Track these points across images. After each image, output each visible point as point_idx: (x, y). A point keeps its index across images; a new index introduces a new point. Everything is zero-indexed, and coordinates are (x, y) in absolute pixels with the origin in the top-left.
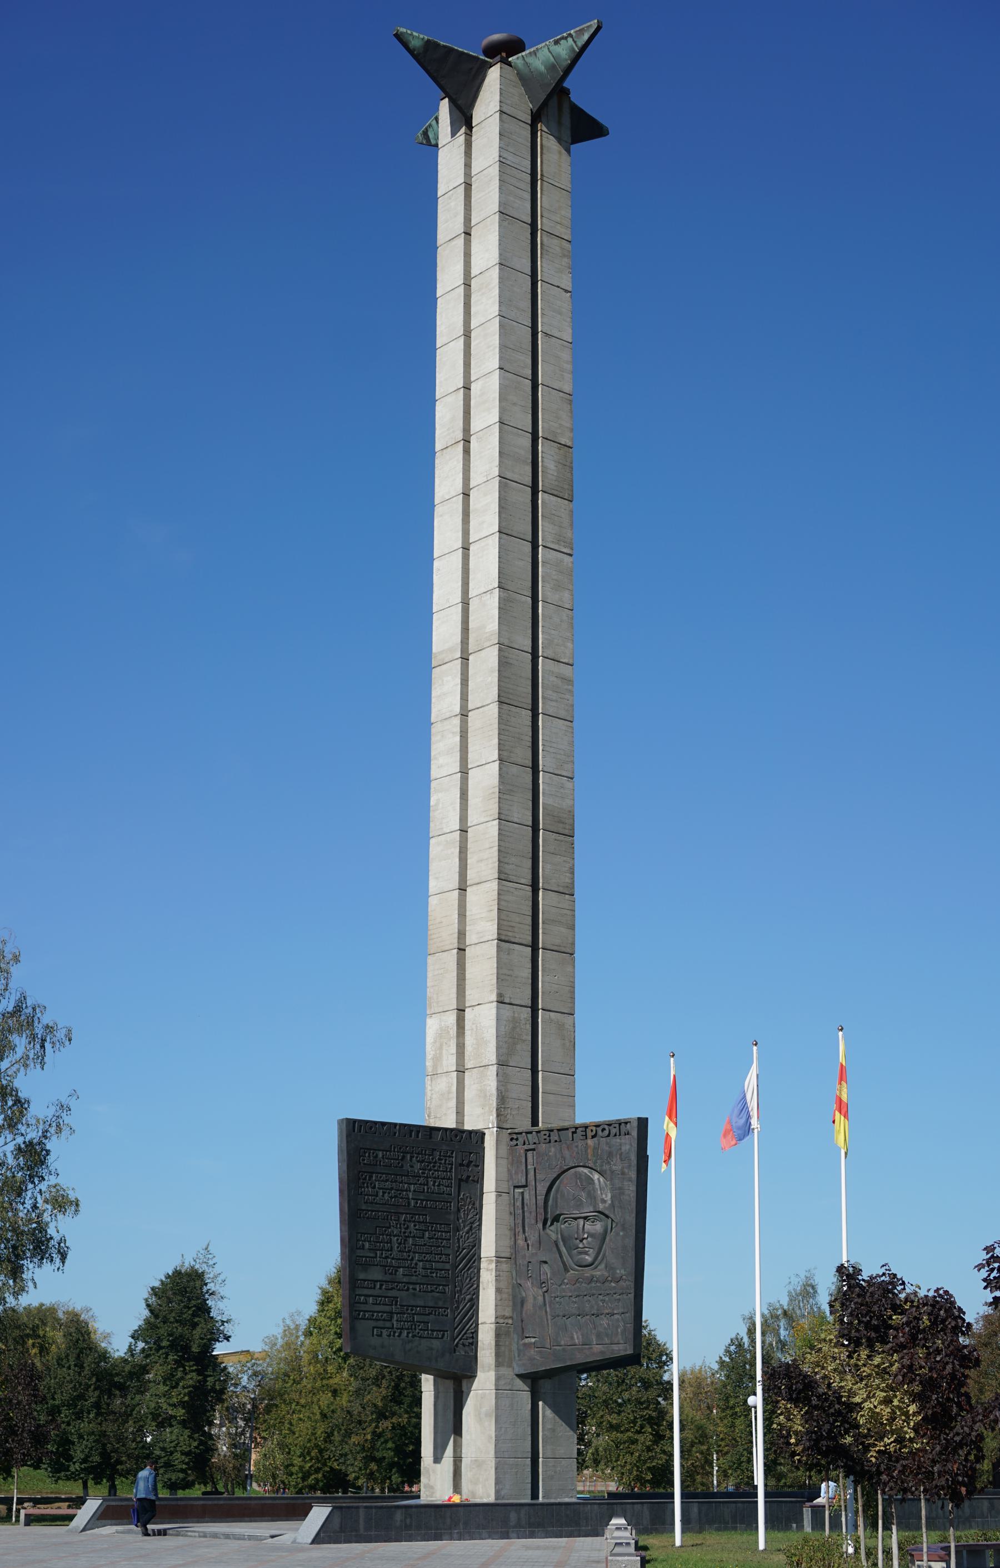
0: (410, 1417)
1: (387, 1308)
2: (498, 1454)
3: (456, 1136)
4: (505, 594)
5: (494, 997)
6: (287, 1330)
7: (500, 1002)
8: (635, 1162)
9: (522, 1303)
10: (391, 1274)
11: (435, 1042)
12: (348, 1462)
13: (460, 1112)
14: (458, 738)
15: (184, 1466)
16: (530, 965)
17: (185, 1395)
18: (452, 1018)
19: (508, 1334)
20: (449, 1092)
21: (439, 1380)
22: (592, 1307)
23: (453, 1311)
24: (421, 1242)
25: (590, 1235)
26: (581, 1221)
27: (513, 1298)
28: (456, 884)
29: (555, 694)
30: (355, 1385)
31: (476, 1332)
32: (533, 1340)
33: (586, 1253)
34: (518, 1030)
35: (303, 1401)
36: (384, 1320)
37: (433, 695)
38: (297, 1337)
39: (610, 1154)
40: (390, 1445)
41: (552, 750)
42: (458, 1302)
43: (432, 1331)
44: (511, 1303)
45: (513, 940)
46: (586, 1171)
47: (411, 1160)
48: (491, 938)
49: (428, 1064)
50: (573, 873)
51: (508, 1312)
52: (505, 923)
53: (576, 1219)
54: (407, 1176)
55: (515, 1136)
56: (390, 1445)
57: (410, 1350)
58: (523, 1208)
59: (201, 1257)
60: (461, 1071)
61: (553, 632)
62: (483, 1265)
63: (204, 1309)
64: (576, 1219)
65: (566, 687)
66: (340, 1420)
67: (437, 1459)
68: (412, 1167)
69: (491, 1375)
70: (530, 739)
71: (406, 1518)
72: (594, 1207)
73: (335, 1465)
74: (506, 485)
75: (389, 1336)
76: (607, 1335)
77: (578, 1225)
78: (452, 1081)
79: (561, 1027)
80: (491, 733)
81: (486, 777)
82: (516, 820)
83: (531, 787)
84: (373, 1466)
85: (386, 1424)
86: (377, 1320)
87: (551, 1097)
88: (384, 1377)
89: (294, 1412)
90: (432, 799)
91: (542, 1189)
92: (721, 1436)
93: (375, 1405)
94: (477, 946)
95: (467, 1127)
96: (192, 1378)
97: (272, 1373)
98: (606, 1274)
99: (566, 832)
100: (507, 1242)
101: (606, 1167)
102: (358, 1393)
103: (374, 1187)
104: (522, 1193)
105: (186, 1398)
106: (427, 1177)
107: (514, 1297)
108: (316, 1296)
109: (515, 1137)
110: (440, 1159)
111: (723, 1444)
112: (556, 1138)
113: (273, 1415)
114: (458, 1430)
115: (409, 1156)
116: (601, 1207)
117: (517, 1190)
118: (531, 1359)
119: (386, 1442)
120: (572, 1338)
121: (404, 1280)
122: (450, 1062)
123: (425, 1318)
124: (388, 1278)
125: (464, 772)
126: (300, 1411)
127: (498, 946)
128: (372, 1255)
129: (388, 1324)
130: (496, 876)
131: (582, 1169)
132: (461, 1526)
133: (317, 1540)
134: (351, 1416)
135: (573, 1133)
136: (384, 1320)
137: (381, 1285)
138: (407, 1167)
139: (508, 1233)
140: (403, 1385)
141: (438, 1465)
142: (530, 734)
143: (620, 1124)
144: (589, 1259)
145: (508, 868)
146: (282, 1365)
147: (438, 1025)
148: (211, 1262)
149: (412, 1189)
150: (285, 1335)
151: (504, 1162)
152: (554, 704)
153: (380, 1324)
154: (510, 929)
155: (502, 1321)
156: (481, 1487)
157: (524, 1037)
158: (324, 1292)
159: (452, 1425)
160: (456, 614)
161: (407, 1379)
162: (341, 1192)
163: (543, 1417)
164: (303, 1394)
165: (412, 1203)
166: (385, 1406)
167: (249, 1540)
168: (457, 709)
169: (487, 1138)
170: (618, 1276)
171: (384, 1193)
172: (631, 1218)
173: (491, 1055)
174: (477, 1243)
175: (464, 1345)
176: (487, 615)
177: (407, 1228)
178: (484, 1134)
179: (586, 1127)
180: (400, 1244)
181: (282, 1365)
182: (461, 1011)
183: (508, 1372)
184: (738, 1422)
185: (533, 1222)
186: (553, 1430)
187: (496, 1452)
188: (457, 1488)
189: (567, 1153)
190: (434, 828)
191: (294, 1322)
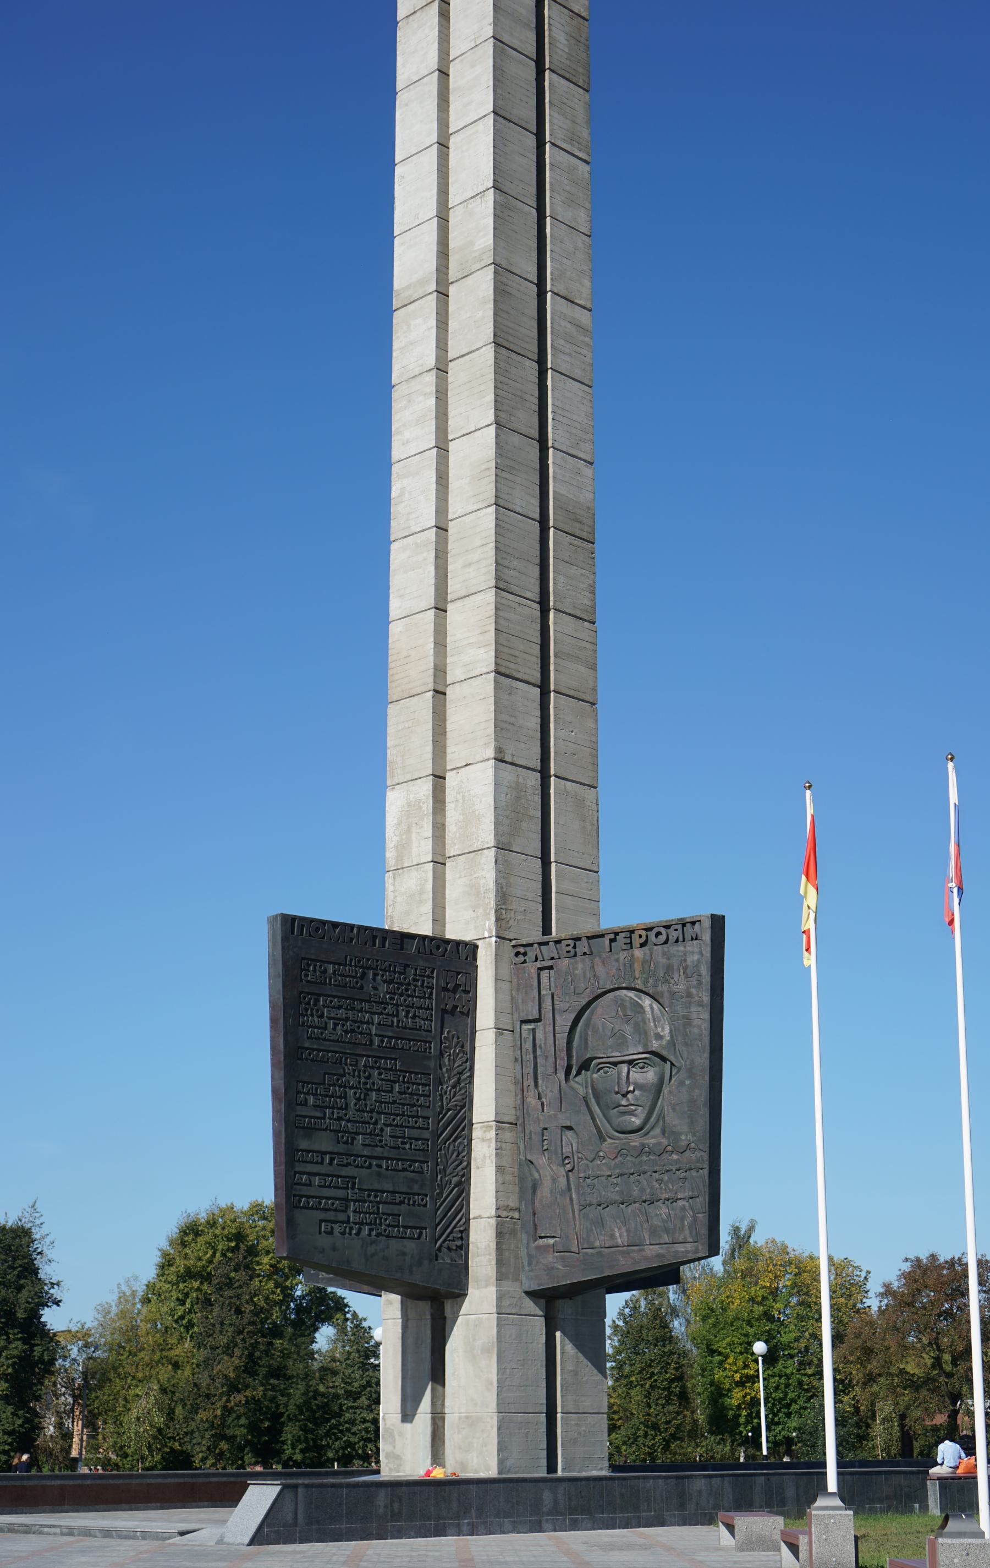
0: (266, 1390)
1: (340, 1193)
2: (503, 1408)
3: (438, 948)
4: (502, 198)
5: (490, 753)
6: (122, 1298)
7: (499, 760)
8: (708, 979)
9: (534, 1188)
10: (346, 1143)
11: (399, 824)
12: (194, 1441)
13: (439, 917)
14: (432, 401)
15: (7, 1447)
16: (538, 713)
17: (8, 1367)
18: (425, 789)
19: (513, 1232)
20: (422, 892)
21: (409, 1302)
22: (643, 1190)
23: (434, 1200)
24: (389, 1097)
25: (637, 1086)
26: (625, 1068)
27: (520, 1181)
28: (429, 598)
29: (568, 346)
30: (202, 1354)
31: (465, 1233)
32: (551, 1241)
33: (632, 1113)
34: (523, 801)
35: (140, 1375)
36: (336, 1210)
37: (394, 347)
38: (134, 1304)
39: (669, 969)
40: (243, 1421)
41: (565, 420)
42: (442, 1187)
43: (405, 1227)
44: (517, 1189)
45: (517, 675)
46: (631, 994)
47: (374, 979)
48: (484, 670)
49: (388, 855)
50: (593, 593)
51: (513, 1202)
52: (506, 650)
53: (615, 1064)
54: (369, 1001)
55: (522, 950)
56: (243, 1421)
57: (373, 1255)
58: (535, 1051)
59: (27, 1215)
60: (439, 862)
61: (565, 261)
62: (477, 1133)
63: (30, 1270)
64: (615, 1064)
65: (582, 338)
66: (186, 1394)
67: (408, 1415)
68: (375, 988)
69: (491, 1293)
70: (536, 401)
71: (392, 1502)
72: (645, 1045)
73: (176, 1446)
74: (503, 51)
75: (343, 1233)
76: (667, 1230)
77: (619, 1074)
78: (433, 870)
79: (580, 802)
80: (482, 387)
81: (476, 449)
82: (518, 509)
83: (538, 466)
84: (224, 1445)
85: (240, 1397)
86: (324, 1209)
87: (568, 900)
88: (236, 1345)
89: (129, 1387)
90: (394, 488)
91: (564, 1022)
92: (615, 1408)
93: (226, 1376)
94: (464, 684)
95: (452, 933)
96: (17, 1347)
97: (105, 1345)
98: (664, 1142)
99: (585, 535)
100: (511, 1100)
101: (663, 988)
102: (207, 1363)
103: (321, 1016)
104: (534, 1030)
105: (10, 1370)
106: (397, 1005)
107: (522, 1179)
108: (156, 1259)
109: (521, 950)
110: (414, 980)
111: (616, 1417)
112: (586, 950)
113: (106, 1390)
114: (438, 1374)
115: (371, 973)
116: (655, 1045)
117: (525, 1027)
118: (550, 1269)
119: (238, 1417)
120: (612, 1236)
121: (365, 1153)
122: (423, 849)
123: (395, 1209)
124: (341, 1148)
125: (442, 447)
126: (137, 1386)
127: (496, 682)
128: (319, 1114)
129: (342, 1217)
130: (493, 583)
131: (625, 992)
132: (474, 1513)
133: (258, 1538)
134: (199, 1390)
135: (611, 941)
136: (336, 1210)
137: (332, 1160)
138: (369, 988)
139: (512, 1087)
140: (257, 1354)
141: (408, 1425)
142: (537, 394)
143: (684, 925)
144: (636, 1121)
145: (509, 574)
146: (116, 1336)
147: (404, 801)
148: (38, 1222)
149: (376, 1021)
150: (120, 1302)
151: (506, 986)
152: (567, 358)
153: (330, 1215)
154: (512, 659)
155: (505, 1214)
156: (475, 1453)
157: (532, 813)
158: (165, 1254)
159: (429, 1367)
160: (430, 233)
161: (262, 1347)
162: (273, 1021)
163: (562, 1353)
164: (140, 1367)
165: (376, 1041)
166: (238, 1377)
167: (144, 1538)
168: (431, 361)
169: (481, 953)
170: (684, 1143)
171: (336, 1025)
172: (702, 1060)
173: (486, 834)
174: (466, 1103)
175: (449, 1249)
176: (476, 228)
177: (369, 1077)
178: (477, 947)
179: (632, 932)
180: (359, 1099)
181: (116, 1336)
182: (439, 778)
183: (515, 1289)
184: (633, 1393)
185: (551, 1070)
186: (576, 1373)
187: (498, 1404)
188: (437, 1456)
189: (600, 970)
190: (396, 528)
191: (130, 1287)
